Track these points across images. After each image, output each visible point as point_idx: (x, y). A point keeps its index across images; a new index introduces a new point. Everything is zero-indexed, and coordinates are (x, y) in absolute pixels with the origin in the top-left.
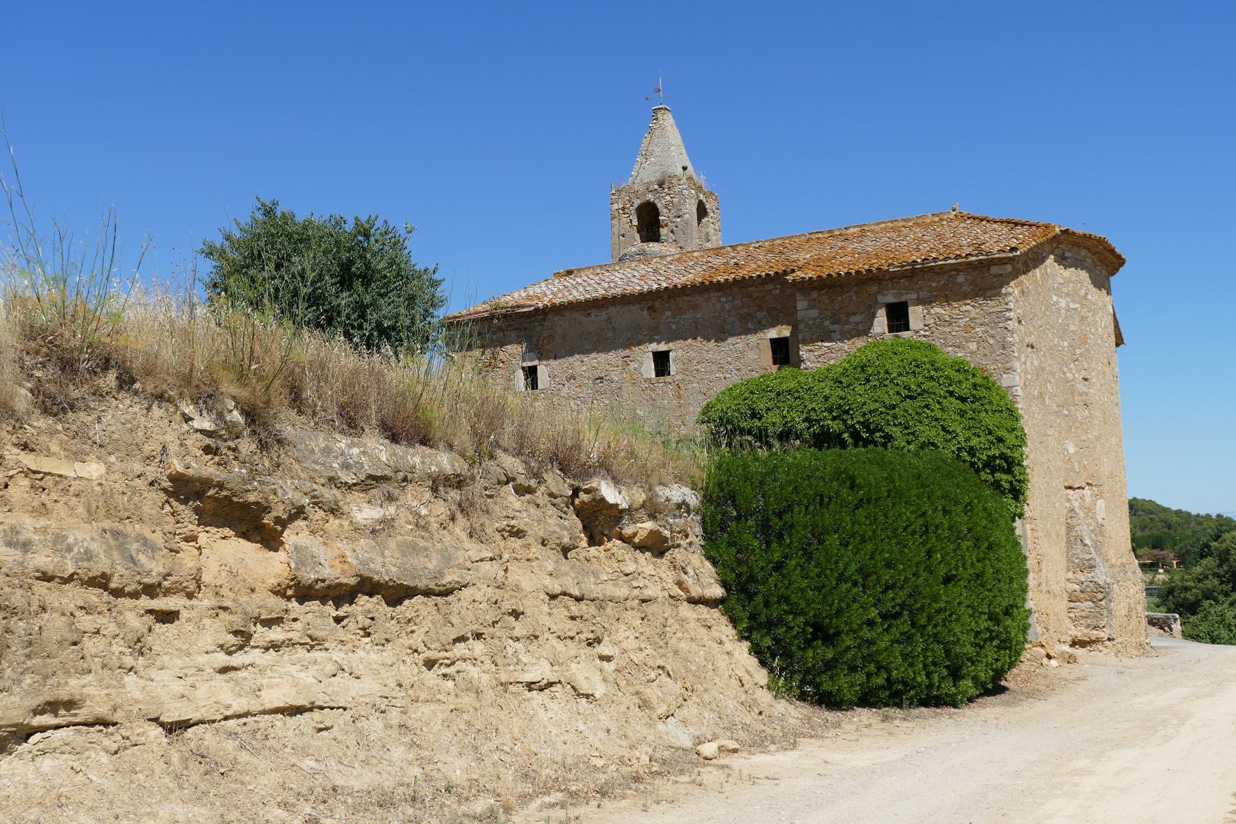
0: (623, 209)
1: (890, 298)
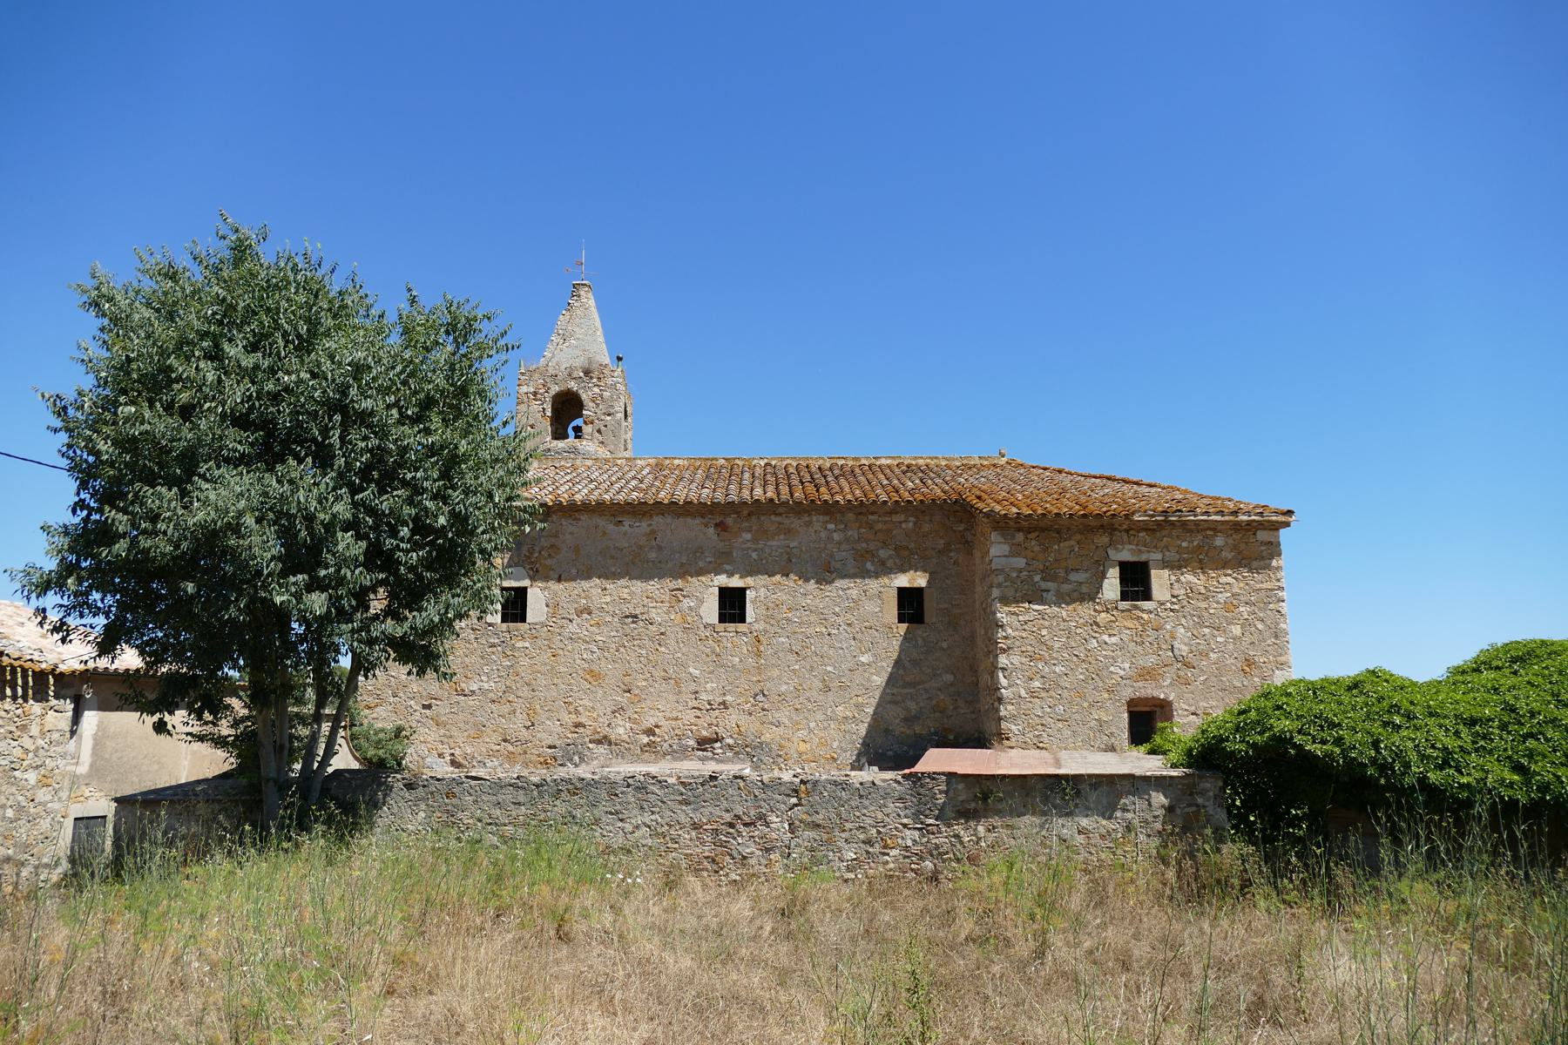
0: (535, 394)
1: (1126, 556)
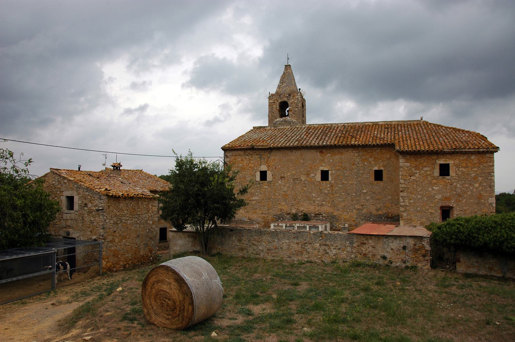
1: (442, 162)
